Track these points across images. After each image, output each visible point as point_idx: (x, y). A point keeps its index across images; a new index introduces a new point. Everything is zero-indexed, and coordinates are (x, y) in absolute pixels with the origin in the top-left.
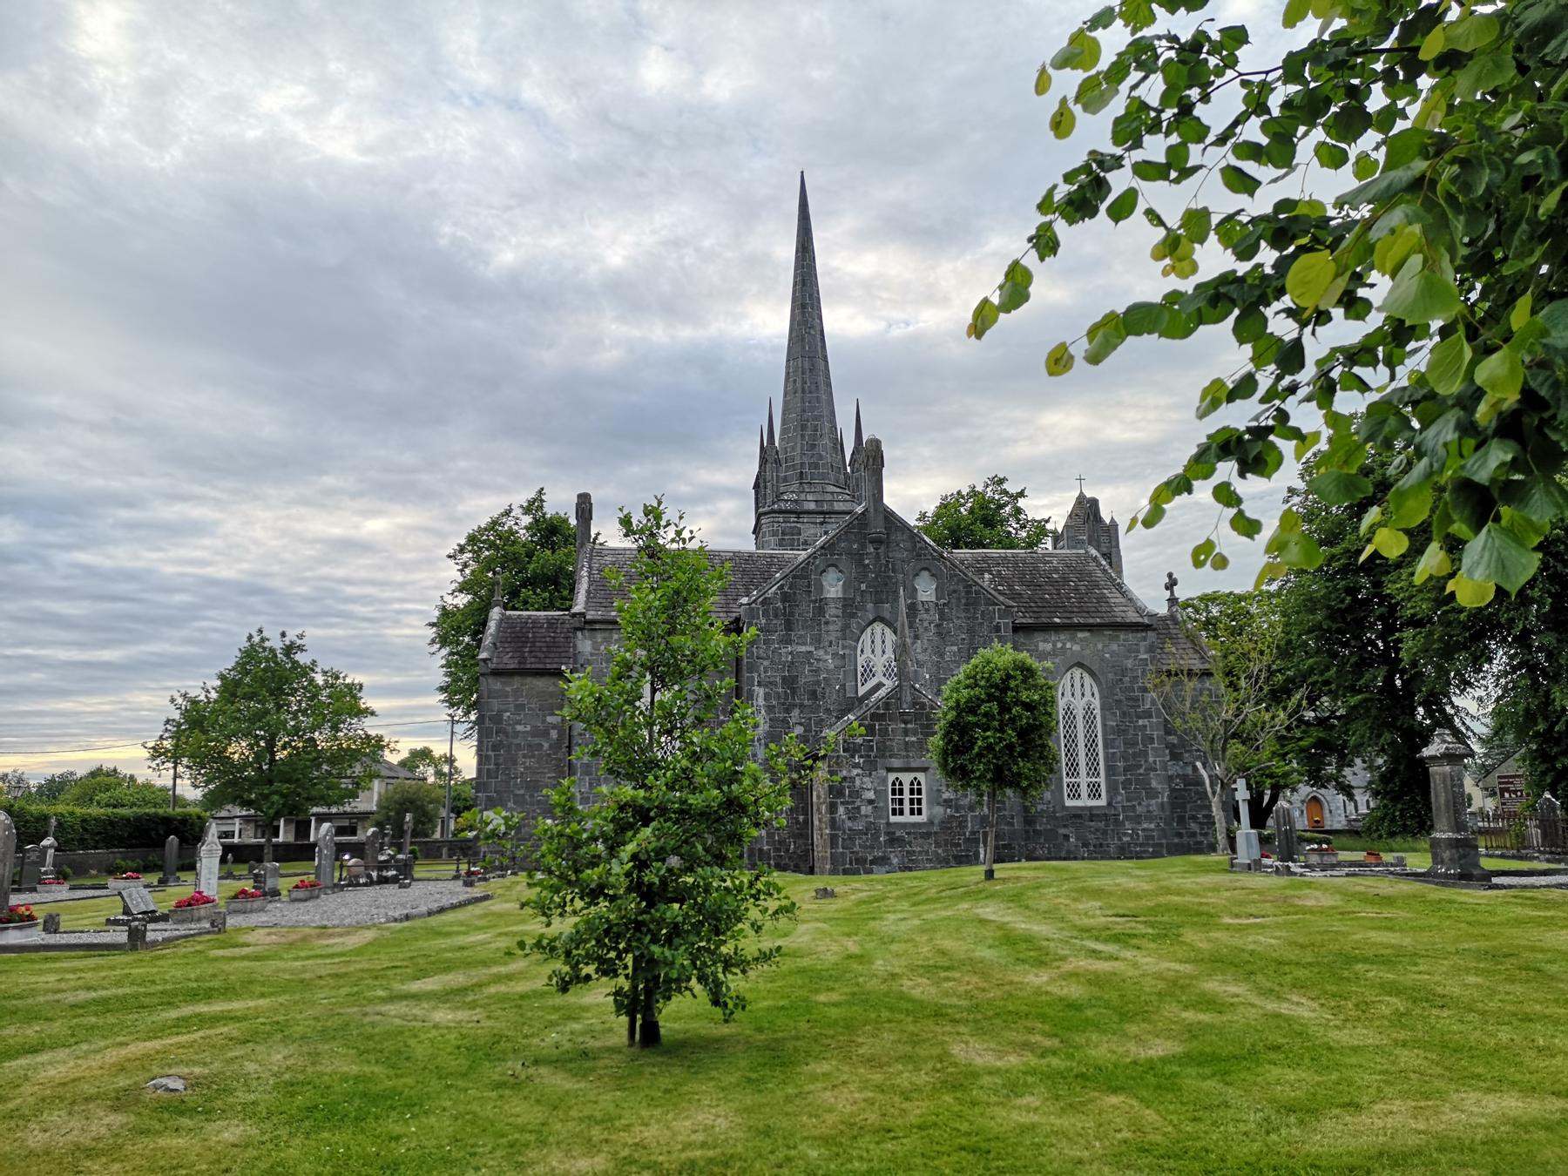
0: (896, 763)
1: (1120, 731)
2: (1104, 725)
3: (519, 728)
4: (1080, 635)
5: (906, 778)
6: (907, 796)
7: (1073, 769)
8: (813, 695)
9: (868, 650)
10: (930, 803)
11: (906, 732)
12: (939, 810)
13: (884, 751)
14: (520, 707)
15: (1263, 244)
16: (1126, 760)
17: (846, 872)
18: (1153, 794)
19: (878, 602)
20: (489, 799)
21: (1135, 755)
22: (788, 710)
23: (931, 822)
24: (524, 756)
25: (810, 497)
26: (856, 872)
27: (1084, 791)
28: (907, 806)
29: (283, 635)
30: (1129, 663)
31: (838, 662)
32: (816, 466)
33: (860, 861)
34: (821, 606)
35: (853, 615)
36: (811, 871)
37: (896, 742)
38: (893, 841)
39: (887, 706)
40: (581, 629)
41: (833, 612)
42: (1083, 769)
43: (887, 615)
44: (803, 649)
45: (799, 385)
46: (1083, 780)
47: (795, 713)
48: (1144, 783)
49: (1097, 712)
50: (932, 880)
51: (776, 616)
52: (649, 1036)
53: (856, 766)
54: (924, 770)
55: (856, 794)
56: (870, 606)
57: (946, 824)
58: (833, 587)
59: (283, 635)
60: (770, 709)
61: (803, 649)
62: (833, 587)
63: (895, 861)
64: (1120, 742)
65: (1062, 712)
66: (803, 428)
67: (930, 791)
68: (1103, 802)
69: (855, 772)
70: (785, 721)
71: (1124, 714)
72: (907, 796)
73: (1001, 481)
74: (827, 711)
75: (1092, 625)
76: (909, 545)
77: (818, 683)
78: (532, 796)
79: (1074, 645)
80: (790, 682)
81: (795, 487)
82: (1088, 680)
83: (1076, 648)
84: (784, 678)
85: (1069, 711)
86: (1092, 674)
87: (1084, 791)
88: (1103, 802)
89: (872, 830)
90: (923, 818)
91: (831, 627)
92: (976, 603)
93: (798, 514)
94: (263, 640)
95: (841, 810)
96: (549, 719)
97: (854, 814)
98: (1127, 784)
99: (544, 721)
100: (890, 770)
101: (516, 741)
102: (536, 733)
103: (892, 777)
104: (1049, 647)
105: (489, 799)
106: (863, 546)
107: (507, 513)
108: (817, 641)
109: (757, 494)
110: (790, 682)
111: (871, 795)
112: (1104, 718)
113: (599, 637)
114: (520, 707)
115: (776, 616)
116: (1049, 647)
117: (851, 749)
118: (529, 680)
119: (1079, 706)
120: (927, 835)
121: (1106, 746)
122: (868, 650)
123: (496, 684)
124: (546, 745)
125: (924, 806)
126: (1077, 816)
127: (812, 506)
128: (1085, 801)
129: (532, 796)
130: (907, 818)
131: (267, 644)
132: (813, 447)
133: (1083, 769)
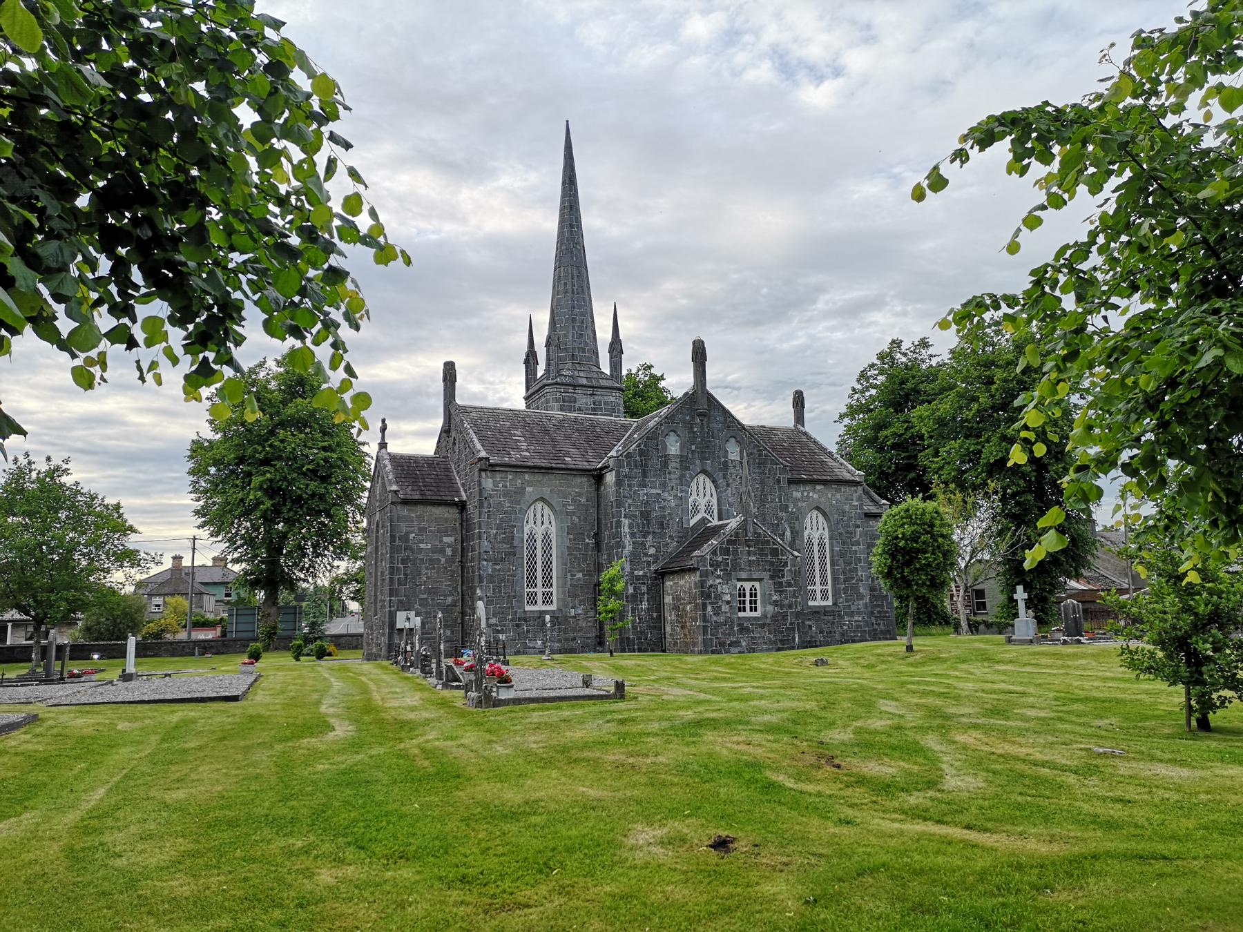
0: (744, 575)
1: (842, 554)
2: (832, 550)
3: (422, 546)
4: (818, 487)
5: (748, 585)
6: (748, 598)
7: (532, 583)
8: (662, 525)
9: (694, 493)
10: (763, 602)
11: (749, 553)
12: (770, 608)
13: (736, 567)
14: (422, 530)
15: (258, 118)
16: (845, 574)
17: (713, 652)
18: (860, 597)
19: (703, 459)
20: (400, 602)
21: (851, 571)
22: (645, 536)
23: (765, 616)
24: (427, 568)
25: (582, 374)
26: (719, 652)
27: (540, 598)
28: (748, 606)
29: (49, 459)
30: (847, 508)
31: (678, 502)
32: (584, 352)
33: (722, 644)
34: (666, 460)
35: (687, 468)
36: (664, 651)
37: (743, 561)
38: (743, 629)
39: (737, 534)
40: (485, 470)
41: (674, 465)
42: (539, 581)
43: (709, 469)
44: (654, 491)
45: (569, 287)
46: (540, 590)
47: (650, 538)
48: (856, 589)
49: (827, 541)
50: (765, 661)
51: (636, 466)
52: (1204, 725)
53: (718, 577)
54: (760, 580)
55: (718, 597)
56: (698, 462)
57: (775, 617)
58: (673, 447)
59: (49, 459)
60: (633, 535)
61: (654, 491)
62: (673, 447)
63: (744, 644)
64: (841, 562)
65: (526, 536)
66: (574, 320)
67: (763, 596)
68: (829, 603)
69: (718, 581)
70: (643, 544)
71: (844, 543)
72: (748, 598)
73: (650, 367)
74: (671, 537)
75: (827, 481)
76: (722, 419)
77: (664, 517)
78: (433, 599)
79: (815, 494)
80: (646, 515)
81: (569, 366)
82: (547, 510)
83: (816, 496)
84: (642, 513)
85: (532, 538)
86: (824, 514)
87: (540, 598)
88: (829, 603)
89: (729, 622)
90: (758, 614)
91: (673, 476)
92: (765, 463)
93: (574, 386)
94: (30, 463)
95: (709, 608)
96: (445, 539)
97: (718, 611)
98: (846, 589)
99: (441, 541)
100: (739, 580)
101: (420, 557)
102: (435, 550)
103: (739, 585)
104: (799, 495)
105: (400, 602)
106: (693, 418)
107: (262, 365)
108: (664, 486)
109: (527, 368)
110: (646, 515)
111: (728, 598)
112: (831, 545)
113: (498, 477)
114: (422, 530)
115: (636, 466)
116: (799, 495)
117: (716, 565)
118: (429, 508)
119: (539, 531)
120: (764, 625)
121: (832, 564)
122: (694, 493)
123: (404, 511)
124: (443, 560)
125: (759, 605)
126: (818, 612)
127: (584, 381)
128: (818, 602)
129: (433, 599)
130: (748, 614)
131: (33, 467)
132: (581, 336)
133: (539, 581)
